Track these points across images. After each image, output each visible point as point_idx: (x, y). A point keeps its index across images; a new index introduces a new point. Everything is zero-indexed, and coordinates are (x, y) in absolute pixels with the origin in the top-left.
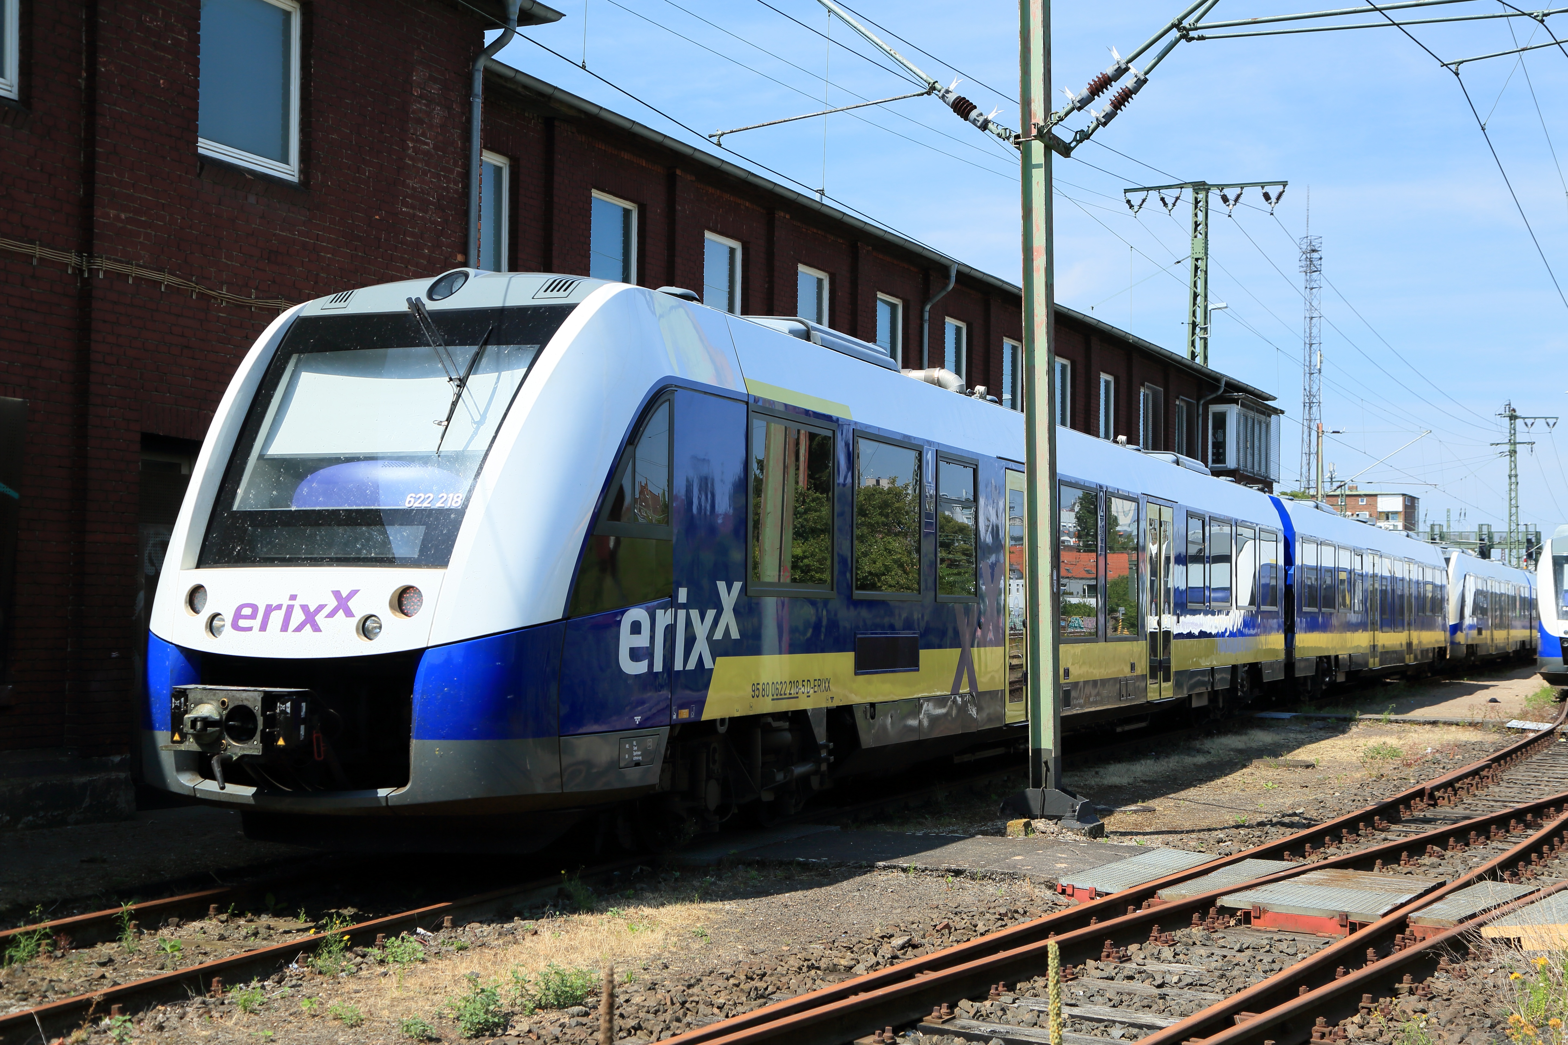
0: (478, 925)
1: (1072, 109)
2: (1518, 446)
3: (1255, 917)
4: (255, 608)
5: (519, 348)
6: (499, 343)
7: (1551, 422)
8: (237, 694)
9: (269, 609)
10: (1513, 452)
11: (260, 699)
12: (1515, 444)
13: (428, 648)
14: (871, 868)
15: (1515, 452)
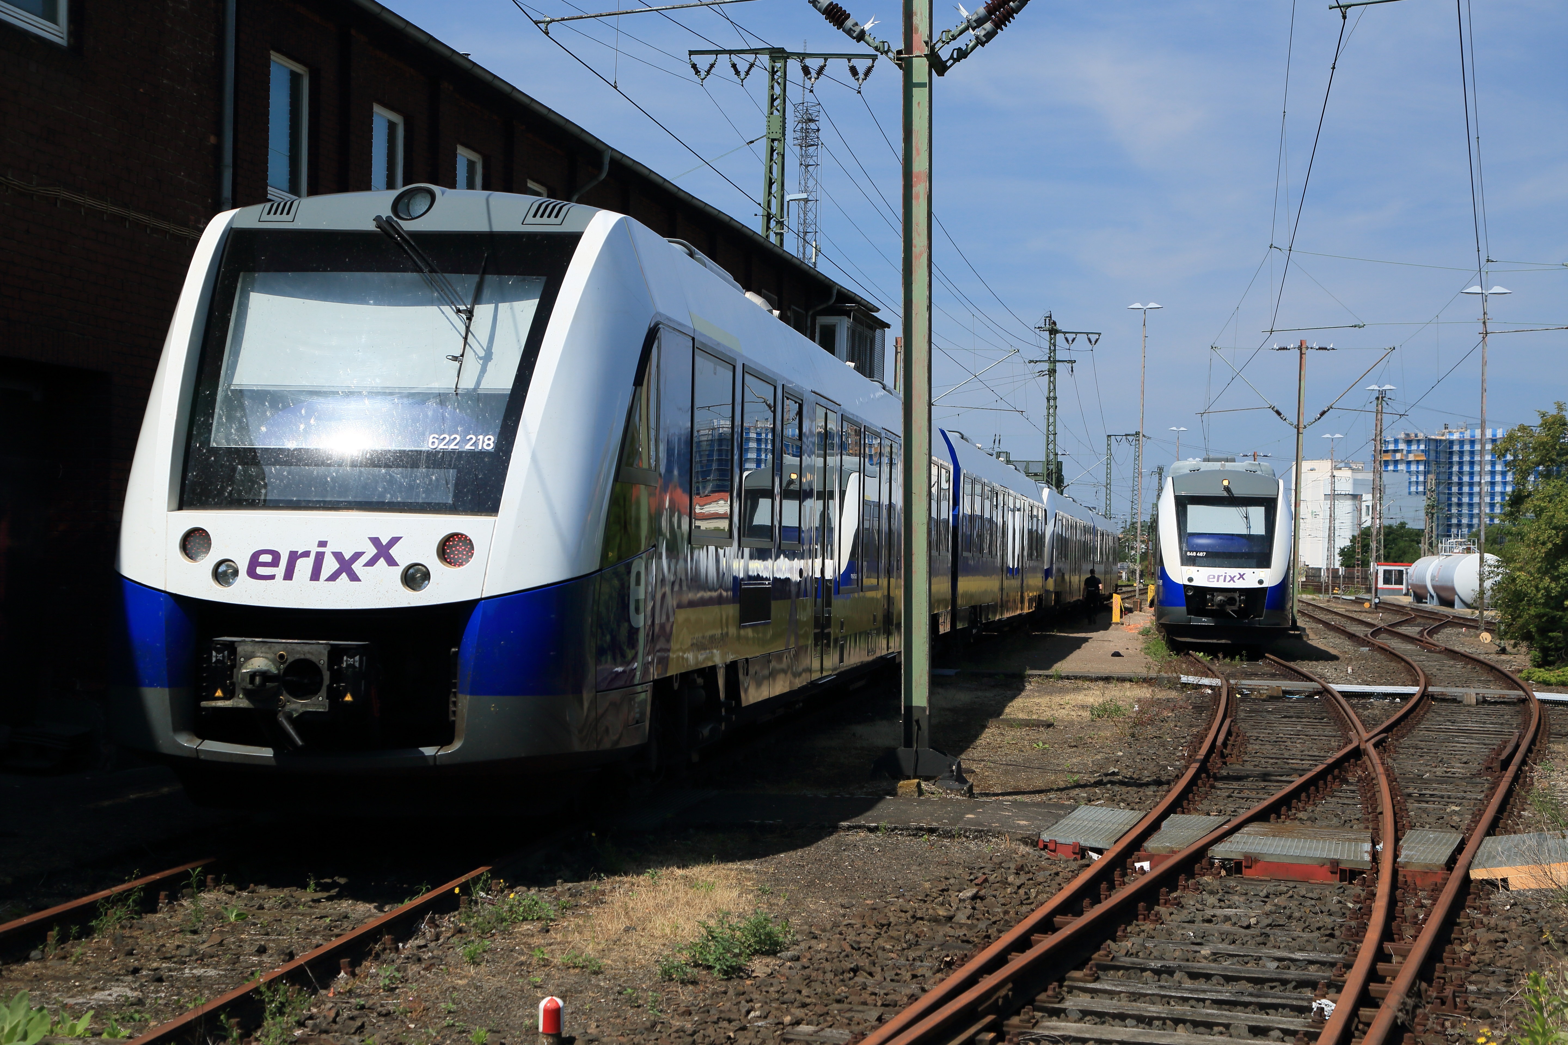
0: (525, 889)
1: (966, 29)
2: (1057, 364)
3: (1246, 867)
4: (276, 556)
5: (524, 280)
6: (499, 272)
7: (1093, 338)
8: (299, 648)
9: (294, 557)
10: (1052, 372)
11: (326, 653)
12: (1055, 361)
13: (481, 599)
14: (834, 829)
15: (1055, 371)
